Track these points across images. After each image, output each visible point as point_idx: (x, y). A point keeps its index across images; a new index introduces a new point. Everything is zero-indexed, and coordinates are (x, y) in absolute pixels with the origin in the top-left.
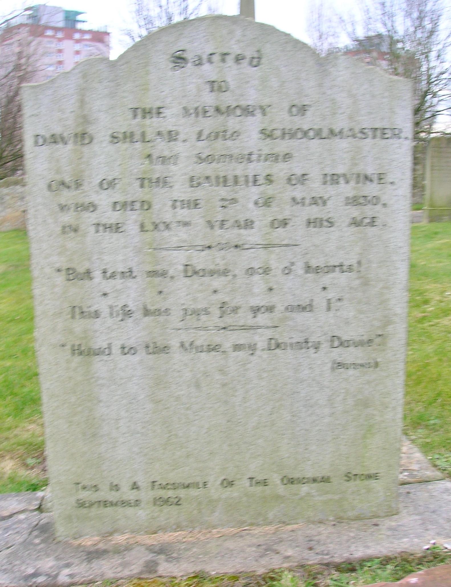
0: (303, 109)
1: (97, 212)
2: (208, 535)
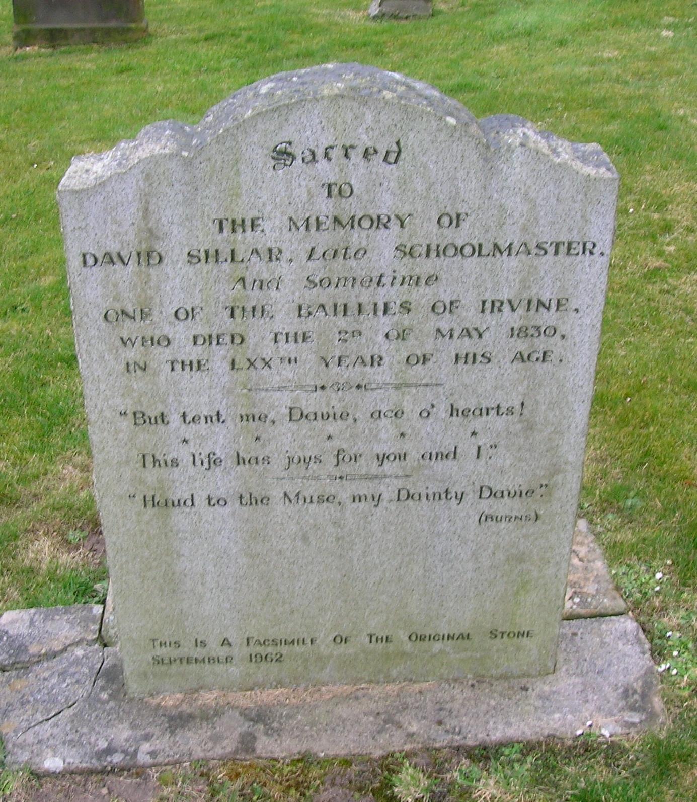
0: (457, 220)
1: (171, 347)
2: (316, 696)
